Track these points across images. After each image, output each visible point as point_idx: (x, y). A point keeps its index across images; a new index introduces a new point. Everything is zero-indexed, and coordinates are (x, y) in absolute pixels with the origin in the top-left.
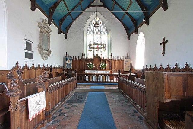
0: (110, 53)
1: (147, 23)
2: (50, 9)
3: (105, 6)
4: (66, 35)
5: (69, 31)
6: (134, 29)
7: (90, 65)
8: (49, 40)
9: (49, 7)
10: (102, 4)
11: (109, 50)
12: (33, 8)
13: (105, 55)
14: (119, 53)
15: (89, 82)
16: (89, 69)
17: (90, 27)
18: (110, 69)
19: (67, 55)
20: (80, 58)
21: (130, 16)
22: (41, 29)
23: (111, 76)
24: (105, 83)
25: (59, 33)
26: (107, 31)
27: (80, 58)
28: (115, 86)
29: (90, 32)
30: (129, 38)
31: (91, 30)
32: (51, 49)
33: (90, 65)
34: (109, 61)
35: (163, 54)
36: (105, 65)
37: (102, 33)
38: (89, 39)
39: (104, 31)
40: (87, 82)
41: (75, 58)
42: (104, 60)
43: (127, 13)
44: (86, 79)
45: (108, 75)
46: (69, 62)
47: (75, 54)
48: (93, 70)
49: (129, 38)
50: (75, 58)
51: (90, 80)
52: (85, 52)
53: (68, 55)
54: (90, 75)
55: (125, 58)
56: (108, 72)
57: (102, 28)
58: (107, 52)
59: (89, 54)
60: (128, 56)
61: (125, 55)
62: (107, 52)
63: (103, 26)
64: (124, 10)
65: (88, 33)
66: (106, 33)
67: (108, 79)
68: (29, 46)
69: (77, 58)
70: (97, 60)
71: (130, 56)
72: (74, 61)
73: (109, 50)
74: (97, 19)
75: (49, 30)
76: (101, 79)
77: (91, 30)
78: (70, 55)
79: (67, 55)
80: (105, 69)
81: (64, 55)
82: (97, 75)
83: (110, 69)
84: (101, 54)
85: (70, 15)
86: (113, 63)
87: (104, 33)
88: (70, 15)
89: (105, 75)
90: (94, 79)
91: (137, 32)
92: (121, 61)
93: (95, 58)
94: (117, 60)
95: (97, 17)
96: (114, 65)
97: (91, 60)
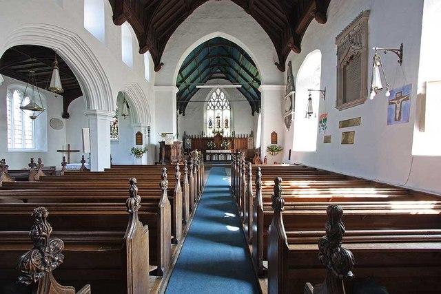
4: (184, 112)
13: (227, 133)
14: (242, 131)
18: (233, 148)
26: (229, 105)
30: (253, 114)
34: (231, 139)
37: (224, 108)
38: (209, 114)
44: (208, 158)
46: (188, 142)
49: (253, 114)
54: (211, 154)
58: (229, 129)
59: (209, 133)
65: (208, 108)
66: (228, 108)
67: (229, 158)
72: (193, 140)
76: (222, 157)
80: (227, 149)
82: (219, 154)
89: (226, 154)
90: (215, 158)
95: (218, 90)
96: (237, 145)
97: (212, 139)
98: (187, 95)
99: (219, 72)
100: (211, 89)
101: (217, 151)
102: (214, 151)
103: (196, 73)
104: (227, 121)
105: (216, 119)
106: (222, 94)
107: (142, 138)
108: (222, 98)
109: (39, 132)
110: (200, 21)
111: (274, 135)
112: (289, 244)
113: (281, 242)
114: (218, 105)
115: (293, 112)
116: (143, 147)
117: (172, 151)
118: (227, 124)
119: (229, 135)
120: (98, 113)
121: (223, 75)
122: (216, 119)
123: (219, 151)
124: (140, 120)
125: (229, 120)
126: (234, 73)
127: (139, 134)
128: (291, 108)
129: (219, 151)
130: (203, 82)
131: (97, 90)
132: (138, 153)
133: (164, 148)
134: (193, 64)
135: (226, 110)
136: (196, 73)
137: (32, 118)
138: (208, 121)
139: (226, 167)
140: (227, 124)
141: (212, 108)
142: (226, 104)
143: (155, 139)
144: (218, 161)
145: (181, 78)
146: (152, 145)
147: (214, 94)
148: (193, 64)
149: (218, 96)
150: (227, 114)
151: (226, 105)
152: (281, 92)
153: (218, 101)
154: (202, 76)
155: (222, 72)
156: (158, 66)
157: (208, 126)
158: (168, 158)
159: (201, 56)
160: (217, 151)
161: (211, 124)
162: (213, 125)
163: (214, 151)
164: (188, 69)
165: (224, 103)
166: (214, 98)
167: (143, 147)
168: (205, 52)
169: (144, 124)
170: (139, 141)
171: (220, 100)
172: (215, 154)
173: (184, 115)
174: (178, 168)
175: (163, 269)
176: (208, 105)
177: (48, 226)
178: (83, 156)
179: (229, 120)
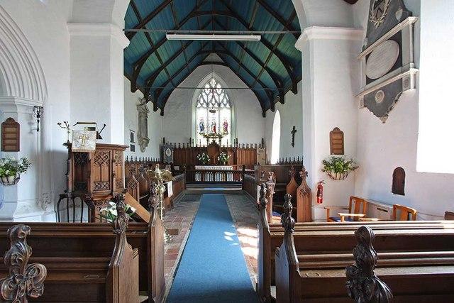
0: (234, 138)
1: (283, 102)
2: (134, 64)
3: (226, 64)
4: (162, 109)
5: (167, 104)
6: (289, 83)
7: (203, 156)
8: (147, 125)
9: (132, 62)
10: (220, 60)
11: (234, 133)
12: (133, 90)
13: (226, 142)
14: (248, 139)
15: (202, 182)
16: (200, 163)
17: (202, 96)
18: (235, 163)
19: (164, 143)
20: (186, 147)
21: (270, 72)
22: (140, 113)
23: (235, 172)
24: (225, 183)
25: (133, 90)
26: (229, 102)
27: (186, 147)
28: (238, 187)
29: (202, 105)
30: (264, 115)
31: (204, 101)
32: (149, 137)
33: (203, 156)
34: (233, 150)
35: (293, 145)
36: (226, 156)
37: (222, 106)
38: (200, 115)
39: (225, 102)
40: (198, 182)
41: (177, 147)
42: (225, 150)
43: (259, 81)
44: (198, 178)
45: (230, 171)
46: (169, 153)
47: (178, 141)
48: (206, 164)
49: (264, 115)
50: (177, 147)
51: (71, 218)
52: (193, 137)
53: (166, 142)
54: (203, 172)
55: (258, 145)
56: (230, 168)
57: (221, 97)
58: (229, 136)
59: (201, 141)
60: (263, 142)
61: (259, 142)
62: (229, 136)
63: (223, 94)
64: (254, 76)
65: (199, 105)
66: (228, 106)
67: (230, 178)
68: (132, 135)
69: (182, 147)
70: (213, 149)
71: (267, 142)
72: (177, 151)
73: (234, 133)
74: (213, 82)
75: (146, 111)
76: (219, 178)
77: (204, 101)
78: (168, 141)
79: (164, 143)
80: (227, 164)
81: (160, 142)
82: (214, 172)
83: (235, 163)
84: (209, 23)
85: (166, 70)
86: (239, 155)
87: (225, 105)
88: (166, 70)
89: (225, 172)
90: (208, 178)
91: (273, 110)
92: (251, 151)
93: (210, 146)
94: (245, 150)
95: (213, 80)
96: (242, 158)
97: (204, 149)
98: (164, 85)
101: (211, 168)
104: (226, 125)
106: (219, 86)
107: (18, 133)
108: (219, 92)
111: (337, 136)
112: (300, 270)
113: (292, 267)
115: (412, 71)
116: (18, 157)
117: (94, 169)
118: (226, 129)
119: (229, 144)
120: (17, 101)
123: (216, 168)
128: (399, 64)
129: (216, 168)
135: (225, 109)
138: (198, 123)
139: (228, 193)
140: (226, 129)
141: (205, 105)
142: (225, 100)
143: (57, 140)
144: (214, 183)
145: (149, 45)
146: (52, 155)
150: (226, 114)
151: (225, 102)
152: (351, 46)
153: (213, 96)
157: (199, 131)
160: (211, 168)
161: (202, 128)
162: (206, 129)
172: (209, 171)
173: (162, 114)
175: (154, 300)
176: (198, 101)
177: (24, 247)
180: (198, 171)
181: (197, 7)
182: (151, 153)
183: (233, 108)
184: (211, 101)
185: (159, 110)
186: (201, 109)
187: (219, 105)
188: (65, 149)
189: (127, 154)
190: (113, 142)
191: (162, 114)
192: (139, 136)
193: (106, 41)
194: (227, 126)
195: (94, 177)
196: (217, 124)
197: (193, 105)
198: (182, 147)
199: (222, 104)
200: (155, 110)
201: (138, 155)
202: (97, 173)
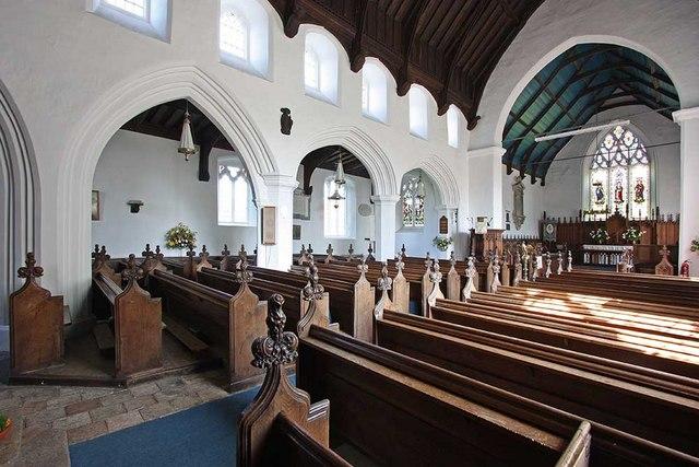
0: (654, 207)
36: (637, 233)
40: (587, 264)
42: (636, 224)
44: (586, 258)
46: (550, 229)
47: (564, 215)
48: (604, 243)
54: (592, 252)
58: (646, 204)
59: (596, 211)
65: (595, 166)
66: (645, 160)
69: (568, 221)
72: (559, 226)
78: (550, 215)
81: (540, 217)
87: (639, 160)
90: (603, 260)
97: (601, 224)
99: (620, 95)
100: (597, 132)
101: (607, 248)
102: (601, 247)
103: (555, 110)
104: (640, 188)
105: (594, 188)
106: (629, 135)
109: (349, 221)
110: (539, 32)
114: (619, 157)
116: (448, 236)
117: (486, 243)
118: (640, 194)
121: (631, 98)
122: (594, 188)
124: (445, 201)
125: (646, 188)
126: (649, 90)
127: (444, 219)
130: (580, 121)
131: (380, 174)
132: (441, 245)
133: (475, 242)
134: (544, 98)
135: (639, 167)
136: (555, 110)
137: (336, 207)
140: (640, 194)
141: (604, 165)
142: (640, 153)
147: (609, 137)
148: (544, 98)
149: (618, 142)
150: (641, 173)
153: (619, 151)
154: (574, 111)
155: (626, 93)
156: (472, 120)
158: (479, 253)
159: (560, 80)
160: (607, 248)
162: (606, 197)
163: (601, 247)
164: (534, 109)
165: (612, 155)
166: (609, 146)
167: (448, 236)
168: (567, 71)
169: (449, 204)
170: (444, 230)
171: (622, 147)
172: (603, 252)
174: (315, 268)
178: (148, 245)
179: (646, 188)
180: (588, 251)
181: (577, 71)
182: (529, 230)
183: (653, 166)
184: (615, 158)
185: (539, 180)
186: (600, 171)
187: (629, 161)
188: (469, 232)
189: (506, 234)
190: (495, 228)
191: (543, 184)
192: (514, 215)
193: (491, 157)
194: (620, 194)
195: (486, 248)
196: (624, 186)
197: (586, 169)
198: (568, 221)
199: (634, 160)
200: (533, 182)
201: (513, 233)
202: (487, 246)
